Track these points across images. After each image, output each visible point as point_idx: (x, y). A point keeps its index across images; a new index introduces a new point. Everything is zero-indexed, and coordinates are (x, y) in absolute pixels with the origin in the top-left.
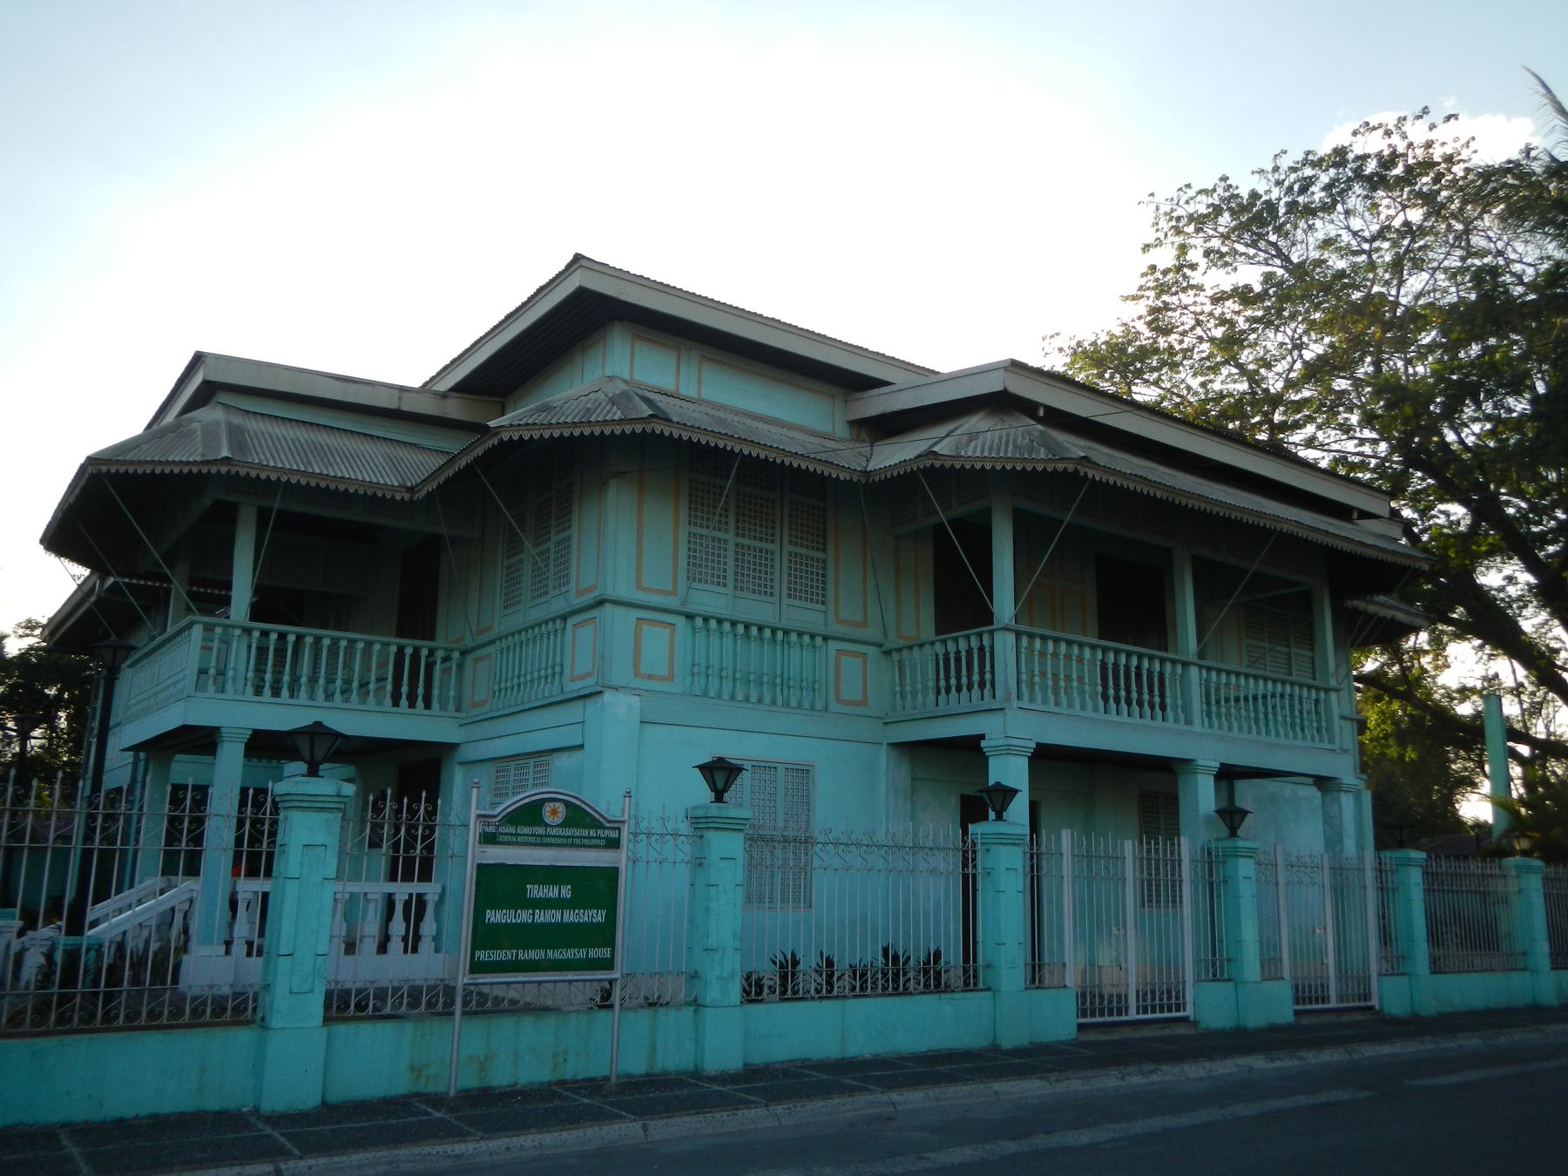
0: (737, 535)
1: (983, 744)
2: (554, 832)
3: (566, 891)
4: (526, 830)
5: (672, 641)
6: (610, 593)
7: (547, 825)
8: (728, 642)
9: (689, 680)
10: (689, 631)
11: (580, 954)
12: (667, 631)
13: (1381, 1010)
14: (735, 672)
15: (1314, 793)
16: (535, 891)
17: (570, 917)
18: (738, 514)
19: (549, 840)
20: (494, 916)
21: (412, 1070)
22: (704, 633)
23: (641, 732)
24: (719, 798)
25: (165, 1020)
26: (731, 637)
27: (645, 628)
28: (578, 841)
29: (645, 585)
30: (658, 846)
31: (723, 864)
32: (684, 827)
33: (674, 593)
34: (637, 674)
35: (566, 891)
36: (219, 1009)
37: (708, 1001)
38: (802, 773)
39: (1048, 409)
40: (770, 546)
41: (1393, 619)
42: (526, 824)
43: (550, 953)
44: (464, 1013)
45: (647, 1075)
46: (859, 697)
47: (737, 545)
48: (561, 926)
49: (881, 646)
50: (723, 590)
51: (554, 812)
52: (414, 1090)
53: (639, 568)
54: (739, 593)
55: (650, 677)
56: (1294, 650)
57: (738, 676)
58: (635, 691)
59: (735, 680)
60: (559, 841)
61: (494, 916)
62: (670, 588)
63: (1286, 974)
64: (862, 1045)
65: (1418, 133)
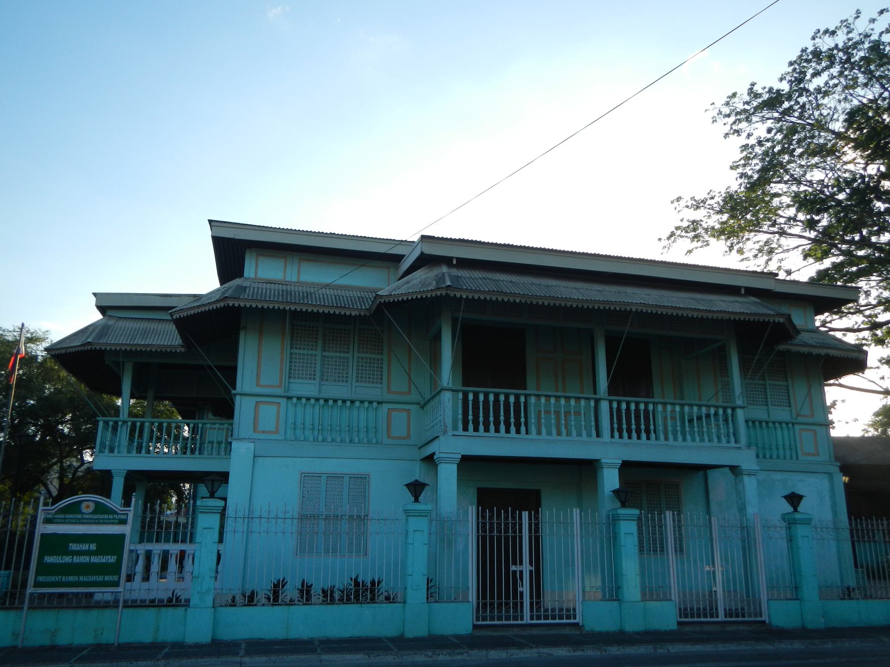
1: (435, 457)
2: (87, 516)
3: (93, 547)
4: (71, 516)
5: (278, 413)
7: (83, 513)
13: (770, 623)
15: (731, 476)
16: (74, 547)
17: (95, 559)
20: (49, 559)
25: (16, 605)
28: (107, 521)
29: (261, 383)
31: (205, 531)
33: (280, 386)
34: (255, 430)
35: (93, 547)
36: (291, 591)
38: (362, 479)
39: (458, 259)
40: (346, 355)
41: (827, 355)
42: (70, 513)
44: (29, 608)
45: (152, 643)
46: (405, 434)
49: (419, 404)
50: (314, 382)
51: (88, 507)
55: (264, 432)
56: (768, 382)
58: (253, 440)
61: (49, 559)
63: (674, 595)
64: (335, 631)
65: (861, 26)
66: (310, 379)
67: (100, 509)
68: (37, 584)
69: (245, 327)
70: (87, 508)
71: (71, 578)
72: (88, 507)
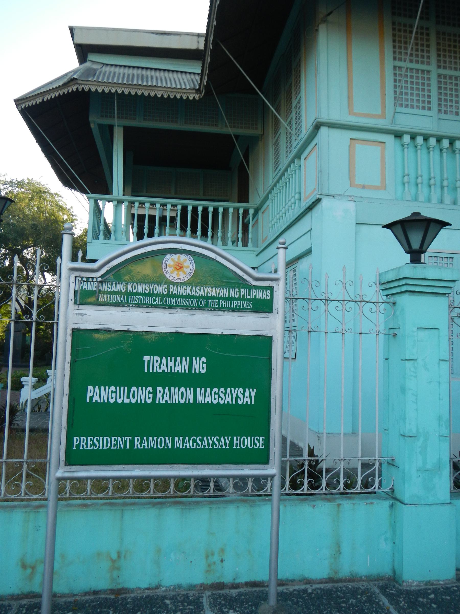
0: (439, 67)
2: (180, 290)
3: (199, 365)
6: (324, 117)
7: (169, 283)
8: (435, 155)
9: (400, 188)
10: (399, 149)
11: (223, 443)
12: (378, 149)
14: (442, 180)
16: (156, 364)
17: (205, 396)
18: (438, 50)
19: (173, 301)
20: (98, 394)
21: (24, 566)
22: (412, 149)
23: (356, 233)
24: (416, 256)
26: (437, 152)
27: (358, 147)
30: (339, 315)
31: (422, 334)
32: (372, 293)
33: (383, 116)
34: (352, 184)
35: (199, 365)
37: (406, 498)
43: (179, 442)
45: (330, 580)
47: (439, 76)
48: (195, 408)
52: (27, 589)
53: (350, 97)
54: (443, 116)
55: (364, 187)
57: (445, 183)
59: (442, 187)
60: (188, 302)
61: (98, 394)
62: (379, 112)
66: (424, 108)
67: (210, 272)
68: (73, 457)
69: (324, 21)
70: (178, 270)
71: (154, 442)
72: (179, 267)
